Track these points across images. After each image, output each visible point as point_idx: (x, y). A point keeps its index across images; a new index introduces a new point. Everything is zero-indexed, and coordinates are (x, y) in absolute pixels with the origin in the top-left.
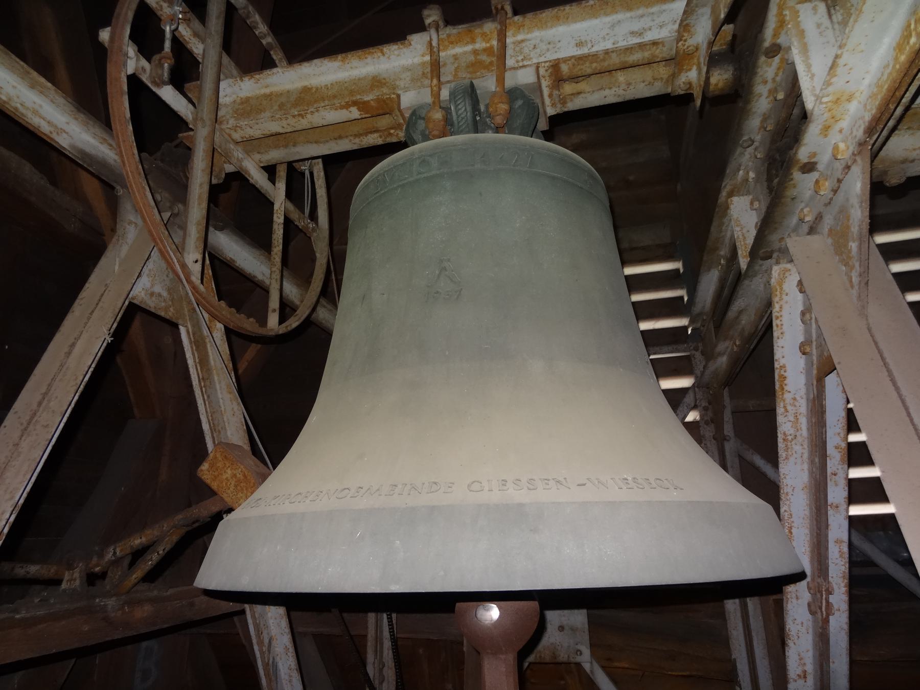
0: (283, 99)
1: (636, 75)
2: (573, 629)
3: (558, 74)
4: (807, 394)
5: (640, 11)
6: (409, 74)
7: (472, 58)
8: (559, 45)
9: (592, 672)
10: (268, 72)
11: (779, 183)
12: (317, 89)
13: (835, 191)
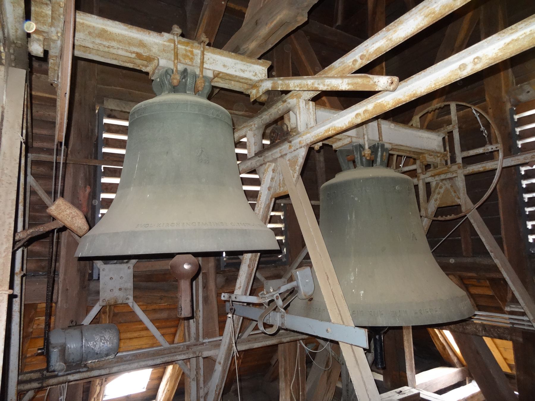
0: (91, 30)
1: (238, 84)
2: (126, 289)
3: (217, 75)
4: (265, 202)
5: (244, 63)
6: (157, 46)
7: (184, 52)
8: (217, 62)
9: (133, 306)
10: (89, 15)
11: (278, 142)
12: (110, 33)
13: (294, 151)
